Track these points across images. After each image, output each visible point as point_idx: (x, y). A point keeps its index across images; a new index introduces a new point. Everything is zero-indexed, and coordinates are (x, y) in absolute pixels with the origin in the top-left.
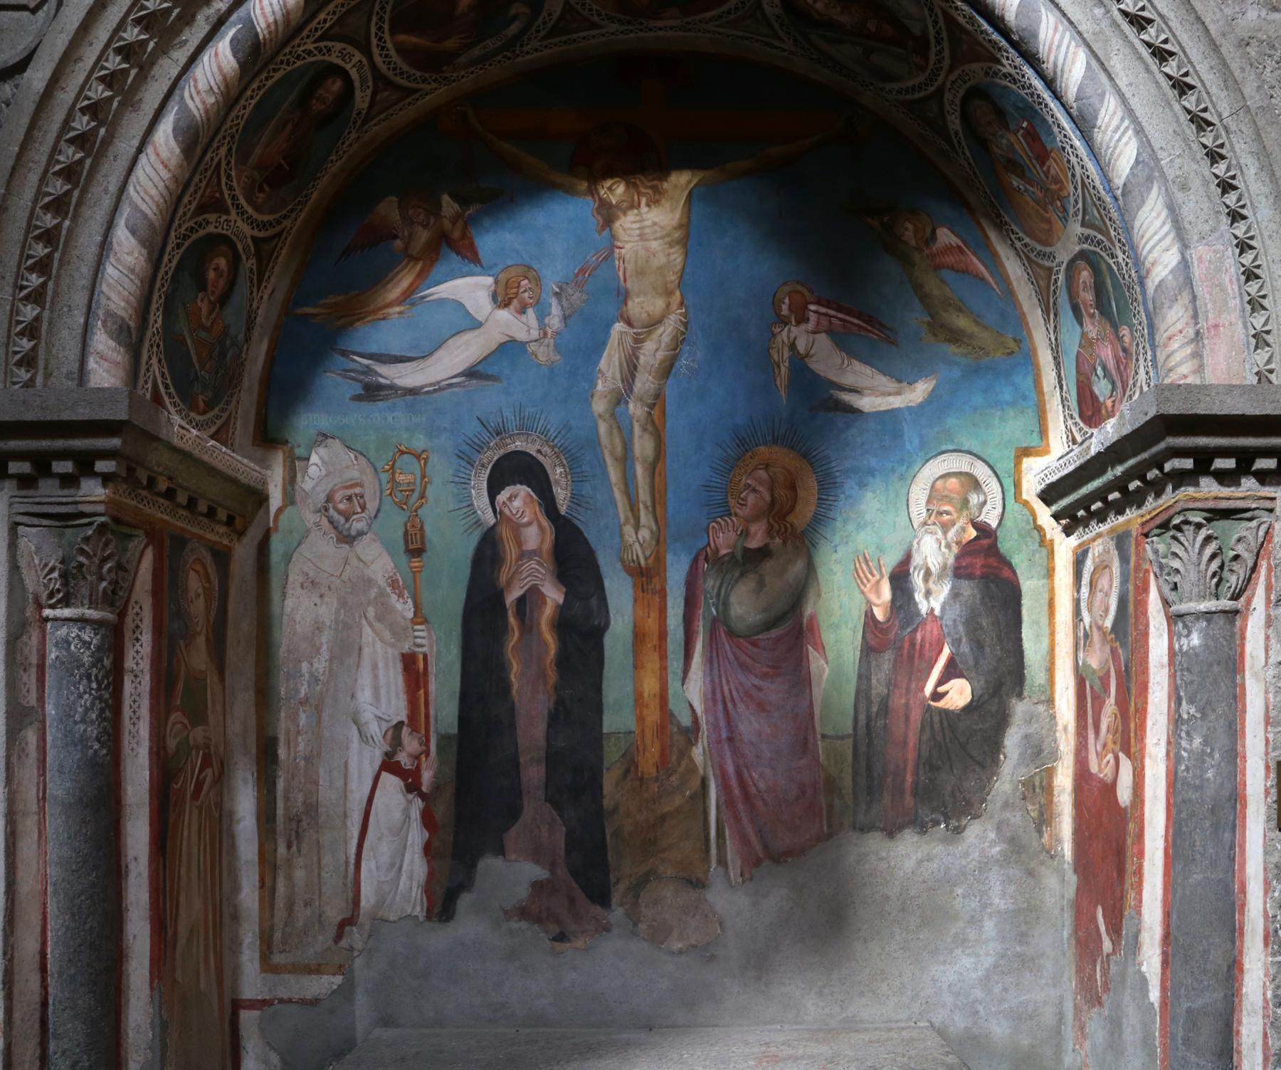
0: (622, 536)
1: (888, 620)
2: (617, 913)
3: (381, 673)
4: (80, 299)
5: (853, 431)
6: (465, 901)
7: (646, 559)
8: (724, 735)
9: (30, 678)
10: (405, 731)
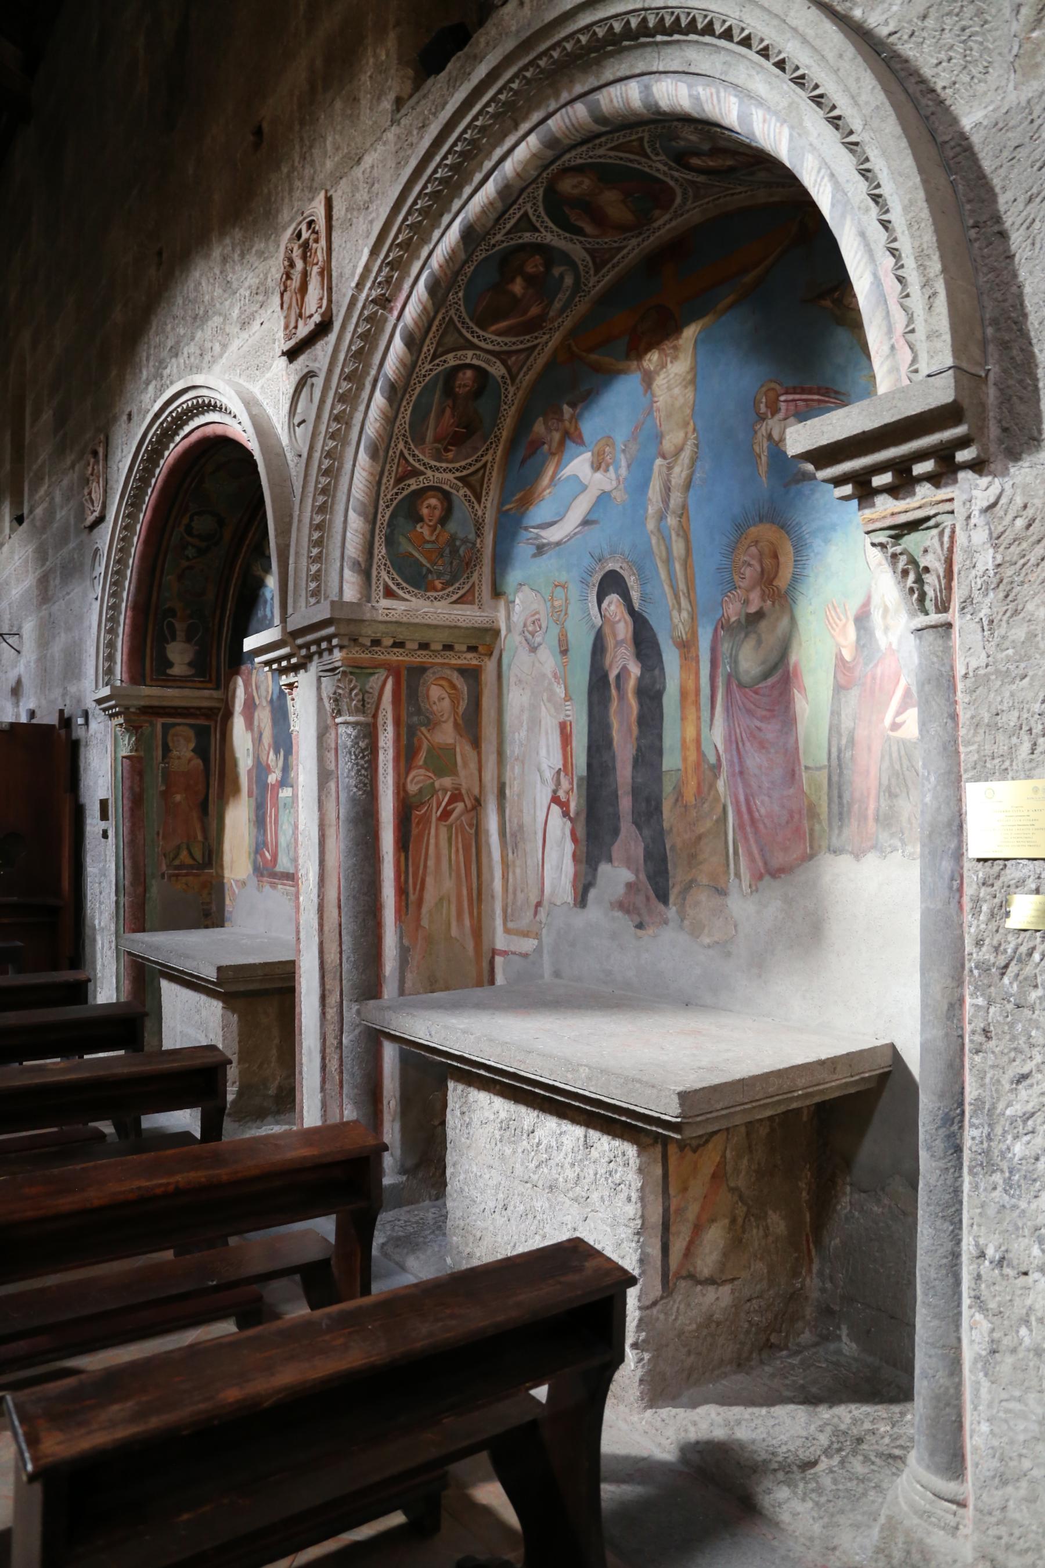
0: (671, 619)
1: (854, 659)
2: (672, 912)
3: (550, 737)
4: (337, 554)
5: (817, 495)
6: (592, 894)
7: (686, 634)
8: (737, 769)
9: (331, 756)
10: (562, 774)
